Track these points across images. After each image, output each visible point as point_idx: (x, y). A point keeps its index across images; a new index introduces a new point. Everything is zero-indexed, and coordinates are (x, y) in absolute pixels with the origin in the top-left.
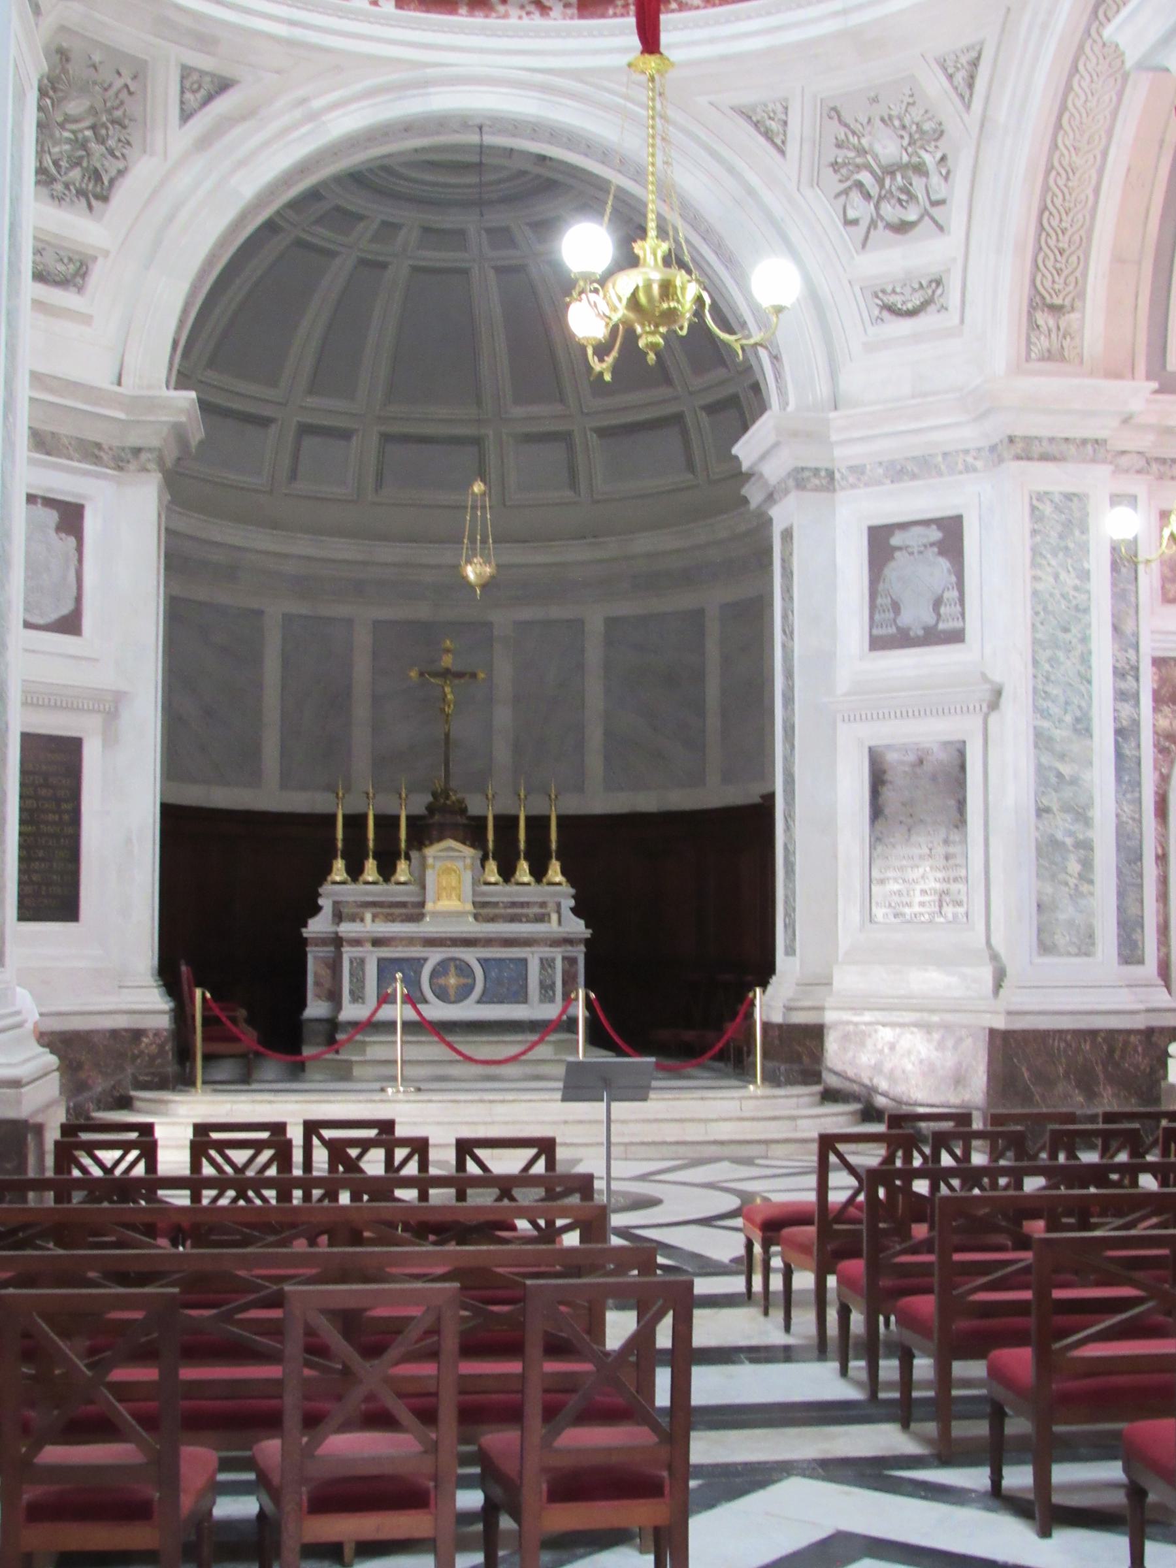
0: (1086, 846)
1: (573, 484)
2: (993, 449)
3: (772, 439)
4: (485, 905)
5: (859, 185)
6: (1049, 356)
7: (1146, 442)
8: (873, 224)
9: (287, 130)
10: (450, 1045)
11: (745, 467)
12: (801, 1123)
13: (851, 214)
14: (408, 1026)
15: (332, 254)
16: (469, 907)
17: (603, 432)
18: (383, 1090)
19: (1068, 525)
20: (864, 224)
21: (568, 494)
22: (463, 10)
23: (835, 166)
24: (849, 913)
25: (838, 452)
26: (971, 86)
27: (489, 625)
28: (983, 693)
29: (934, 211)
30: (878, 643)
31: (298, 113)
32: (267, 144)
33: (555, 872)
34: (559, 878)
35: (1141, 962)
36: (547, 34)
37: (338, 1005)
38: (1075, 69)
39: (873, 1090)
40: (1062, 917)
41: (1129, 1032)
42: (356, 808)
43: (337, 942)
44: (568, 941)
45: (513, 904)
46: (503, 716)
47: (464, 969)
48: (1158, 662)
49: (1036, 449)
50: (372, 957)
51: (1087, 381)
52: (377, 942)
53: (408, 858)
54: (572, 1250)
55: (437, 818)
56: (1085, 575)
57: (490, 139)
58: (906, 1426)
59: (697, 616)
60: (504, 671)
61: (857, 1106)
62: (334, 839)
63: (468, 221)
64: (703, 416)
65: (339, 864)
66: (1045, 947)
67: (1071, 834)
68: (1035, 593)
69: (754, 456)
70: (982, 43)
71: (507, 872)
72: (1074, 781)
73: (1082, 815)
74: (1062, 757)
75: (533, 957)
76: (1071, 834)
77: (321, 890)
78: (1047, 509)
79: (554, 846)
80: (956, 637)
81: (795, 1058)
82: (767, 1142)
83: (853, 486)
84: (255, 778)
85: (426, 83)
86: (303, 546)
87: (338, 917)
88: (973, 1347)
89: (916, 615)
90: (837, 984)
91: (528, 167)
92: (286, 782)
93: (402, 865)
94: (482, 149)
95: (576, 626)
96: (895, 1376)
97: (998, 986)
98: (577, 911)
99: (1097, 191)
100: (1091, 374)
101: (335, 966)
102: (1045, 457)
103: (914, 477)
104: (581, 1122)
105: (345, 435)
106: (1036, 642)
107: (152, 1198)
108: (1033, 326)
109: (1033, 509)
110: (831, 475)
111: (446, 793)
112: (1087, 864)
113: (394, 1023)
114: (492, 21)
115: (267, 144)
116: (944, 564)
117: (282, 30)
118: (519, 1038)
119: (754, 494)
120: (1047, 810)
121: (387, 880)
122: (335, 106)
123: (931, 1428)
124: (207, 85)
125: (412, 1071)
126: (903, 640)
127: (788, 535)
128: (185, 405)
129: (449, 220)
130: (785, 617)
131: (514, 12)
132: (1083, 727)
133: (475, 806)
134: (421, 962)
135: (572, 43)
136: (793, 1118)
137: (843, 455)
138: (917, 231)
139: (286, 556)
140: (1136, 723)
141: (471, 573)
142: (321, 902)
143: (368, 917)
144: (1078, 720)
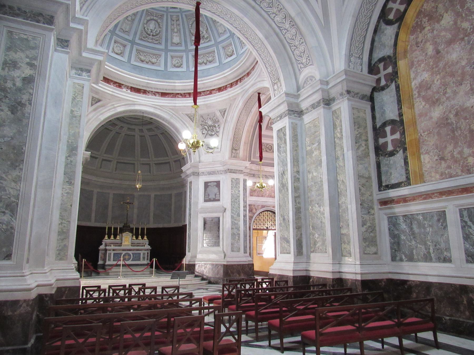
0: (239, 234)
1: (150, 172)
2: (225, 171)
3: (189, 167)
4: (132, 243)
5: (205, 128)
6: (234, 157)
7: (248, 171)
8: (207, 134)
9: (109, 110)
10: (130, 268)
11: (183, 171)
12: (193, 281)
13: (203, 132)
14: (123, 265)
15: (111, 131)
16: (130, 244)
17: (155, 164)
18: (118, 277)
19: (237, 183)
20: (205, 134)
21: (149, 174)
22: (142, 93)
23: (201, 125)
24: (199, 245)
25: (200, 170)
26: (224, 115)
27: (134, 195)
28: (223, 209)
29: (217, 133)
30: (205, 201)
31: (112, 107)
32: (106, 111)
33: (145, 238)
34: (146, 239)
35: (247, 253)
36: (156, 99)
37: (105, 262)
38: (241, 114)
39: (203, 275)
40: (235, 246)
41: (245, 265)
42: (110, 226)
43: (106, 250)
44: (147, 250)
45: (138, 243)
46: (136, 211)
47: (129, 255)
48: (249, 205)
49: (232, 171)
50: (112, 253)
51: (240, 161)
52: (114, 250)
53: (119, 235)
54: (102, 304)
55: (125, 228)
56: (239, 191)
57: (144, 115)
58: (247, 335)
59: (171, 195)
60: (136, 203)
61: (201, 278)
62: (106, 231)
63: (137, 128)
64: (174, 163)
65: (106, 236)
66: (232, 251)
67: (237, 232)
68: (232, 194)
69: (186, 170)
70: (226, 109)
71: (137, 238)
72: (237, 224)
73: (238, 229)
74: (235, 220)
75: (142, 253)
76: (237, 232)
77: (103, 241)
78: (234, 181)
79: (140, 233)
80: (219, 200)
81: (190, 270)
82: (188, 285)
83: (202, 175)
84: (90, 220)
85: (135, 104)
86: (102, 180)
87: (106, 245)
88: (262, 321)
89: (212, 196)
90: (197, 257)
91: (149, 120)
92: (96, 221)
93: (118, 236)
94: (143, 116)
95: (149, 196)
96: (245, 325)
97: (225, 257)
98: (149, 244)
99: (243, 133)
100: (240, 160)
101: (105, 254)
102: (233, 173)
103: (212, 174)
104: (155, 282)
105: (110, 161)
106: (231, 201)
107: (113, 301)
108: (232, 152)
109: (232, 180)
110: (198, 173)
111: (127, 224)
112: (239, 237)
113: (120, 265)
114: (146, 96)
115: (106, 111)
116: (217, 189)
117: (111, 93)
118: (143, 267)
119: (183, 176)
120: (233, 228)
121: (115, 239)
122: (118, 107)
123: (254, 335)
124: (96, 100)
125: (123, 273)
126: (210, 200)
127: (191, 183)
128: (89, 154)
129: (133, 127)
130: (190, 196)
131: (150, 95)
132: (239, 215)
133: (132, 226)
134: (121, 254)
135: (160, 101)
136: (191, 280)
137: (201, 170)
138: (214, 136)
139: (99, 181)
140: (246, 215)
141: (137, 186)
142: (103, 243)
143: (112, 245)
144: (238, 214)
